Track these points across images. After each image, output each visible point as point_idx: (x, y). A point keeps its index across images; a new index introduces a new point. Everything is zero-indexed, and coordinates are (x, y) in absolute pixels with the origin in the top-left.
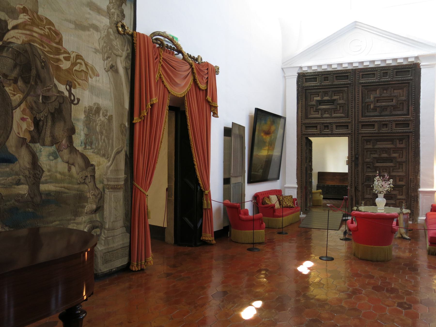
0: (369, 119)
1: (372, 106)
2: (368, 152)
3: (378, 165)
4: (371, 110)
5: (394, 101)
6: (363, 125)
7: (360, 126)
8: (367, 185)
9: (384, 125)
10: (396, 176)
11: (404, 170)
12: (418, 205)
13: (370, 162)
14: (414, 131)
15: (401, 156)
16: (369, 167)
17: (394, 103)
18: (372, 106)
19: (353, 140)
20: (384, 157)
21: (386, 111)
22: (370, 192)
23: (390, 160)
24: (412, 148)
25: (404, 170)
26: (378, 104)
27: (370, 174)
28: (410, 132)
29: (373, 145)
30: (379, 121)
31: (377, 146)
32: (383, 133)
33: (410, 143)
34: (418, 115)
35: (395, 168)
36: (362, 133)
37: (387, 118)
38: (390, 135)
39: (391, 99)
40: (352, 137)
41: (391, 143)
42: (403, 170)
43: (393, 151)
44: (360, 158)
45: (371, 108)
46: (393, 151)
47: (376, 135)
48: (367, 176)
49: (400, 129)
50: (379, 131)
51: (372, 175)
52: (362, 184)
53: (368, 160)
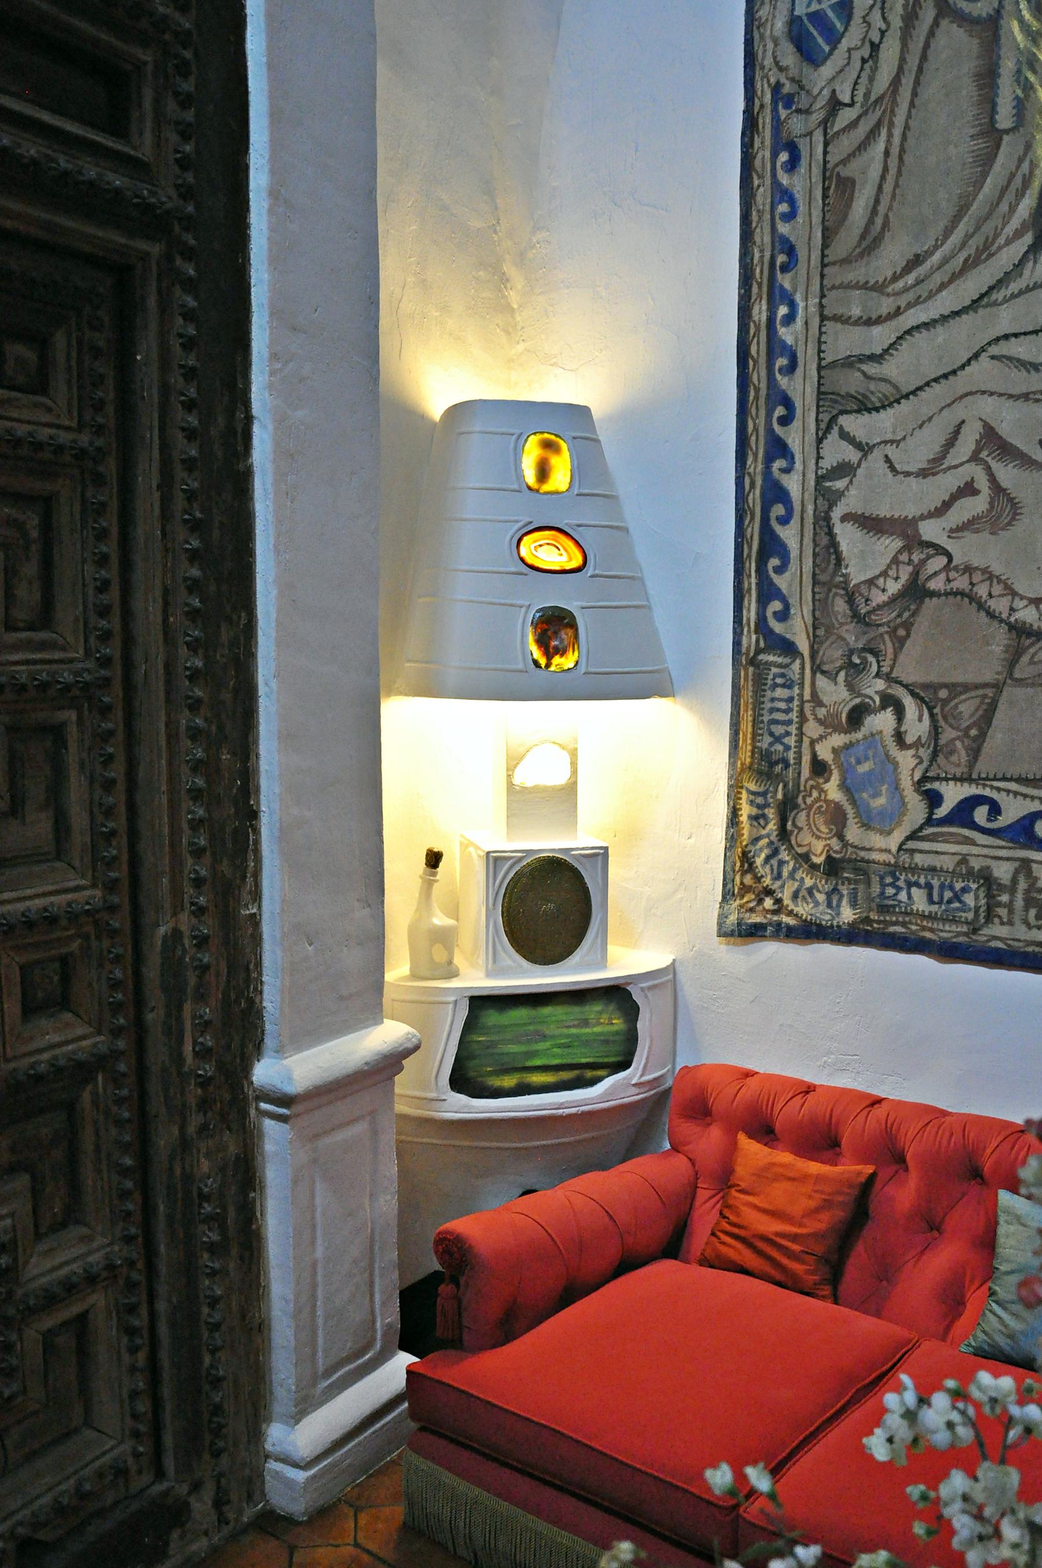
25: (79, 819)
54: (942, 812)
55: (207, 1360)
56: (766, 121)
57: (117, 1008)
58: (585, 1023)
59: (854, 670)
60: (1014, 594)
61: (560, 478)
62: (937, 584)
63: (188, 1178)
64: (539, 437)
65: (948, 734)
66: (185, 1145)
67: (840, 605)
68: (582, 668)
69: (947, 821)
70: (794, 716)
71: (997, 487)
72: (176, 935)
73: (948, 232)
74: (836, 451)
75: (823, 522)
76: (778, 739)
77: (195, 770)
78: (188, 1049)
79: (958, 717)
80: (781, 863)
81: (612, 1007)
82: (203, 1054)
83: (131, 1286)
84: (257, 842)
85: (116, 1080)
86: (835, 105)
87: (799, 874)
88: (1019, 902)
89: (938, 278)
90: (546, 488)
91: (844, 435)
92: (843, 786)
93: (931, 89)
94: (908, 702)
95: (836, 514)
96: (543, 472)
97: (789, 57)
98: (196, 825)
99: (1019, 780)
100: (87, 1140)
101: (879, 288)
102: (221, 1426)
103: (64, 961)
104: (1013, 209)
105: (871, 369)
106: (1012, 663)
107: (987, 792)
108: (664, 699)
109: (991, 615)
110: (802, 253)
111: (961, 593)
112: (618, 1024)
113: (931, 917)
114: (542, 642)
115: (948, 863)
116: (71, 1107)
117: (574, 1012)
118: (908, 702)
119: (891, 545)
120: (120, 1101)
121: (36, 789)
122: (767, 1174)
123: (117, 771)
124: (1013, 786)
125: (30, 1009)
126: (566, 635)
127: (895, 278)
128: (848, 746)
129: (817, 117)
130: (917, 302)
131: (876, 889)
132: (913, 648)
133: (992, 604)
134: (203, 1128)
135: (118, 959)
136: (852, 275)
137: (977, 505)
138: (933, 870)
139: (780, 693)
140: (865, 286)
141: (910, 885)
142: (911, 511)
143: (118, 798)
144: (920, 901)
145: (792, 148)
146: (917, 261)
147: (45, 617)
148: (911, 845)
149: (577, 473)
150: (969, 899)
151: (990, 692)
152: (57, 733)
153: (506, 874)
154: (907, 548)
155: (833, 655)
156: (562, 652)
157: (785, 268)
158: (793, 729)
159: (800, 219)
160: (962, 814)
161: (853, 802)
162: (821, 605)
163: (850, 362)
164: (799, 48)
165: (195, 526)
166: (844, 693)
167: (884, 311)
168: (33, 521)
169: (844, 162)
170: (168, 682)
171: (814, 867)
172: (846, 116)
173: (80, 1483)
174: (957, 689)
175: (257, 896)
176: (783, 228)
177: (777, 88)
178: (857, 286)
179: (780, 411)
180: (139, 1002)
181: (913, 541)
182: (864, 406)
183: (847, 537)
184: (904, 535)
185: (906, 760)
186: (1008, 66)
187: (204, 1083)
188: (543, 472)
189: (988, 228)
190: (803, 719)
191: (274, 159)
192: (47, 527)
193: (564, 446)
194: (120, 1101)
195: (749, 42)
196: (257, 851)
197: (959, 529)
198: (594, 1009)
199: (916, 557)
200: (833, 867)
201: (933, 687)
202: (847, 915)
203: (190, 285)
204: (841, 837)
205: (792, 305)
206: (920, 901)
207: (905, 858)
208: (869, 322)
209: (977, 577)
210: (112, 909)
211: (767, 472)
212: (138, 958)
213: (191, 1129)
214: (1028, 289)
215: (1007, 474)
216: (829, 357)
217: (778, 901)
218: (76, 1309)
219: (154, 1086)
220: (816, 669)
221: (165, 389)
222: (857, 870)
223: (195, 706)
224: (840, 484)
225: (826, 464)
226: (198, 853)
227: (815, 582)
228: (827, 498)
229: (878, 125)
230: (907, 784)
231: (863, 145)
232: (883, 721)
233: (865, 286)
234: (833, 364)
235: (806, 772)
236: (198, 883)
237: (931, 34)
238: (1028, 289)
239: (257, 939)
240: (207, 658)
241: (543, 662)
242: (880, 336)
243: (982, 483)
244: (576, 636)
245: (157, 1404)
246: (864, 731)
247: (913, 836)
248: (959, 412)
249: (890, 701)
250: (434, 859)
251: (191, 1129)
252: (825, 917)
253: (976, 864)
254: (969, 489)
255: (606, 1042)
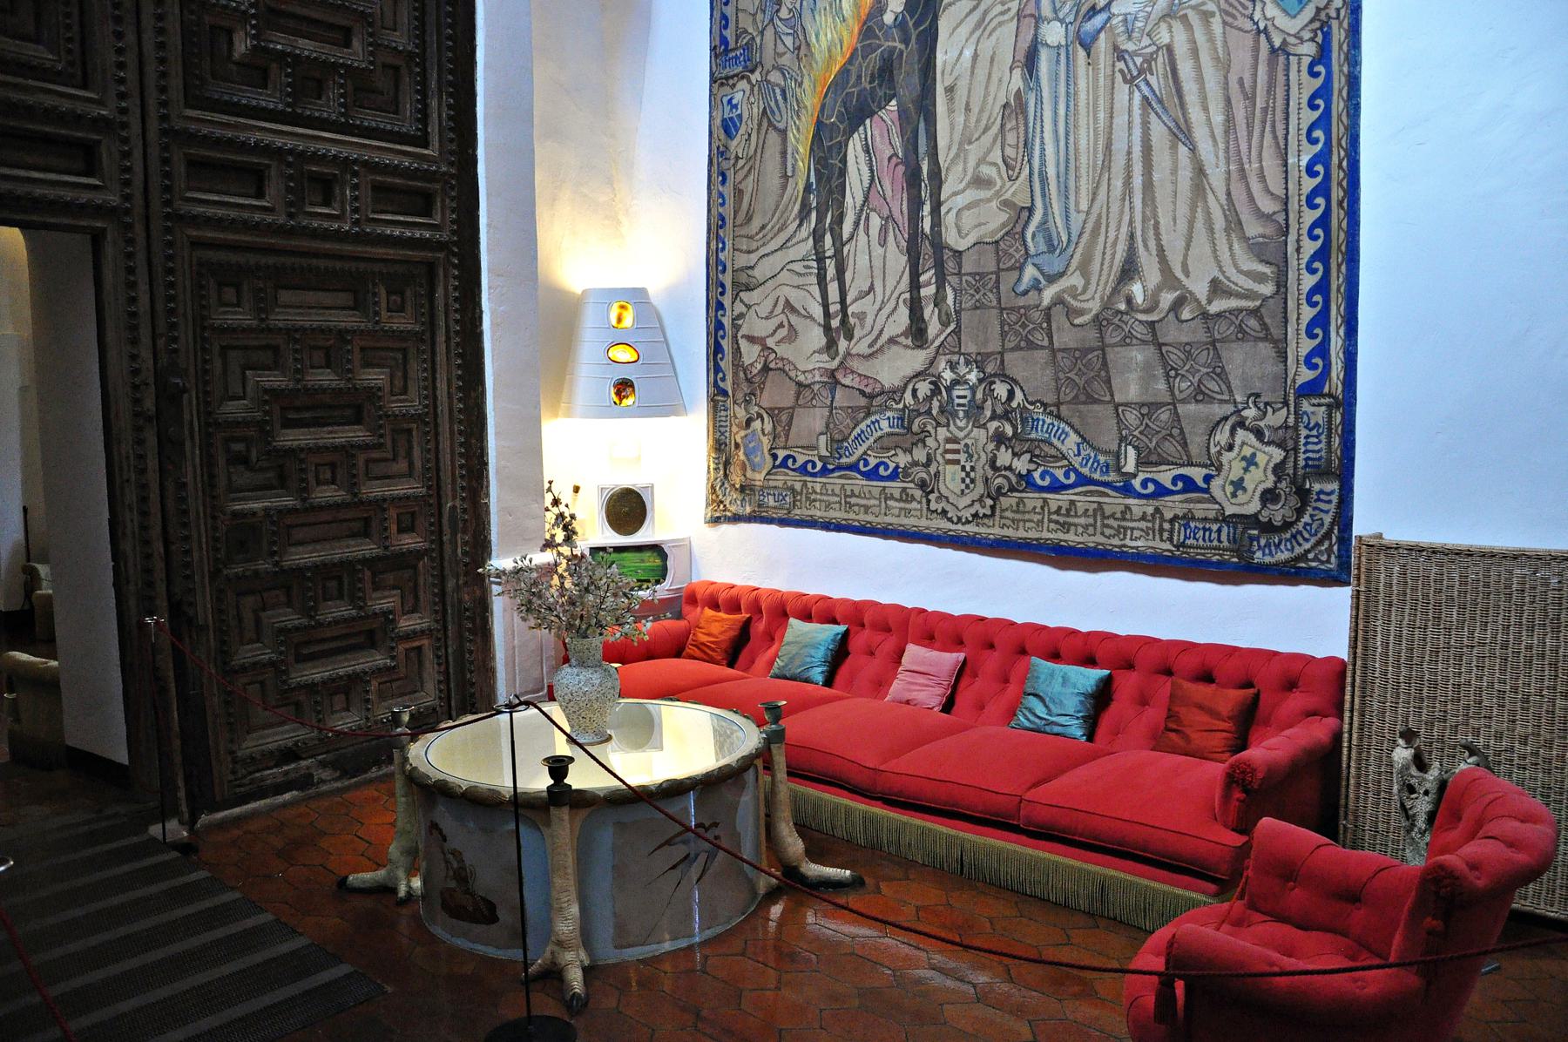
0: (236, 126)
1: (242, 45)
2: (232, 354)
3: (292, 438)
4: (234, 68)
5: (356, 43)
6: (194, 164)
7: (180, 169)
8: (238, 577)
9: (315, 178)
10: (385, 500)
11: (418, 464)
12: (490, 649)
13: (246, 423)
14: (455, 243)
15: (398, 383)
16: (243, 460)
17: (356, 54)
18: (242, 45)
19: (140, 260)
20: (324, 390)
21: (320, 98)
22: (258, 621)
23: (355, 406)
24: (448, 339)
25: (418, 464)
26: (279, 43)
27: (256, 506)
28: (440, 246)
29: (261, 310)
30: (291, 152)
31: (280, 319)
32: (315, 234)
33: (441, 308)
34: (470, 151)
35: (375, 455)
36: (194, 220)
37: (331, 144)
38: (231, 237)
39: (341, 28)
40: (131, 242)
41: (343, 298)
42: (411, 465)
43: (362, 349)
44: (190, 400)
45: (236, 55)
46: (362, 349)
47: (247, 238)
48: (235, 514)
49: (396, 224)
50: (291, 216)
51: (266, 509)
52: (215, 574)
53: (233, 409)
54: (778, 463)
55: (468, 676)
56: (715, 161)
57: (432, 533)
58: (643, 561)
59: (748, 402)
60: (797, 369)
61: (628, 320)
62: (772, 365)
63: (460, 601)
64: (618, 304)
65: (779, 429)
66: (458, 588)
67: (742, 375)
68: (636, 404)
69: (779, 467)
70: (728, 423)
71: (790, 325)
72: (454, 508)
73: (773, 216)
74: (739, 308)
75: (735, 337)
76: (722, 434)
77: (461, 446)
78: (459, 550)
79: (781, 421)
80: (726, 489)
81: (655, 554)
82: (465, 553)
83: (439, 640)
84: (488, 475)
85: (432, 559)
86: (737, 158)
87: (732, 493)
88: (804, 499)
89: (770, 235)
90: (621, 326)
91: (741, 301)
92: (746, 454)
93: (767, 154)
94: (765, 416)
95: (739, 335)
96: (619, 320)
97: (723, 136)
98: (461, 467)
99: (802, 447)
100: (421, 581)
101: (751, 238)
102: (474, 704)
103: (413, 514)
104: (792, 209)
105: (750, 272)
106: (797, 398)
107: (792, 453)
108: (673, 419)
109: (790, 378)
110: (727, 221)
111: (780, 369)
112: (658, 562)
113: (775, 508)
114: (618, 394)
115: (780, 484)
116: (415, 568)
117: (638, 555)
118: (765, 416)
119: (757, 348)
120: (433, 568)
121: (402, 452)
122: (711, 620)
123: (431, 446)
124: (800, 450)
125: (400, 531)
126: (629, 390)
127: (757, 234)
128: (746, 436)
129: (732, 162)
130: (764, 244)
131: (757, 498)
132: (765, 393)
133: (790, 373)
134: (466, 583)
135: (432, 515)
136: (742, 233)
137: (783, 332)
138: (775, 487)
139: (723, 413)
140: (747, 237)
141: (768, 494)
142: (763, 334)
143: (431, 456)
144: (772, 503)
145: (723, 175)
146: (763, 227)
147: (405, 391)
148: (768, 477)
149: (637, 318)
150: (787, 499)
151: (791, 410)
152: (409, 431)
153: (607, 495)
154: (762, 350)
155: (740, 396)
156: (627, 397)
157: (721, 227)
158: (728, 429)
159: (726, 206)
160: (784, 464)
161: (748, 459)
162: (735, 374)
163: (742, 269)
164: (725, 131)
165: (459, 355)
166: (744, 413)
167: (754, 248)
168: (400, 356)
169: (740, 183)
170: (450, 413)
171: (736, 489)
172: (741, 163)
173: (419, 708)
174: (781, 410)
175: (488, 495)
176: (721, 210)
177: (718, 148)
178: (743, 236)
179: (720, 290)
180: (441, 532)
181: (765, 348)
182: (749, 289)
183: (743, 343)
184: (762, 345)
185: (765, 440)
186: (789, 151)
187: (466, 565)
188: (619, 320)
189: (785, 216)
190: (731, 425)
191: (489, 211)
192: (405, 358)
193: (629, 307)
194: (433, 568)
195: (710, 126)
196: (487, 477)
197: (779, 342)
198: (646, 555)
199: (766, 354)
200: (743, 489)
201: (772, 409)
202: (748, 510)
203: (455, 266)
204: (745, 476)
205: (724, 243)
206: (772, 503)
207: (766, 482)
208: (749, 252)
209: (785, 361)
210: (430, 496)
211: (716, 316)
212: (440, 514)
213: (461, 582)
214: (798, 243)
215: (794, 319)
216: (736, 267)
217: (725, 506)
218: (417, 644)
219: (446, 564)
220: (735, 403)
221: (446, 305)
222: (751, 490)
223: (460, 422)
224: (740, 322)
225: (735, 313)
226: (462, 477)
227: (733, 365)
228: (736, 327)
229: (750, 169)
230: (766, 451)
231: (746, 176)
232: (757, 424)
233: (747, 237)
234: (736, 271)
235: (733, 448)
236: (463, 488)
237: (766, 133)
238: (798, 243)
239: (488, 513)
240: (465, 404)
241: (618, 402)
242: (754, 257)
243: (786, 323)
244: (634, 391)
245: (449, 690)
246: (751, 429)
247: (768, 474)
248: (778, 292)
249: (760, 416)
250: (576, 490)
251: (461, 582)
252: (740, 512)
253: (789, 484)
254: (781, 325)
255: (653, 570)
